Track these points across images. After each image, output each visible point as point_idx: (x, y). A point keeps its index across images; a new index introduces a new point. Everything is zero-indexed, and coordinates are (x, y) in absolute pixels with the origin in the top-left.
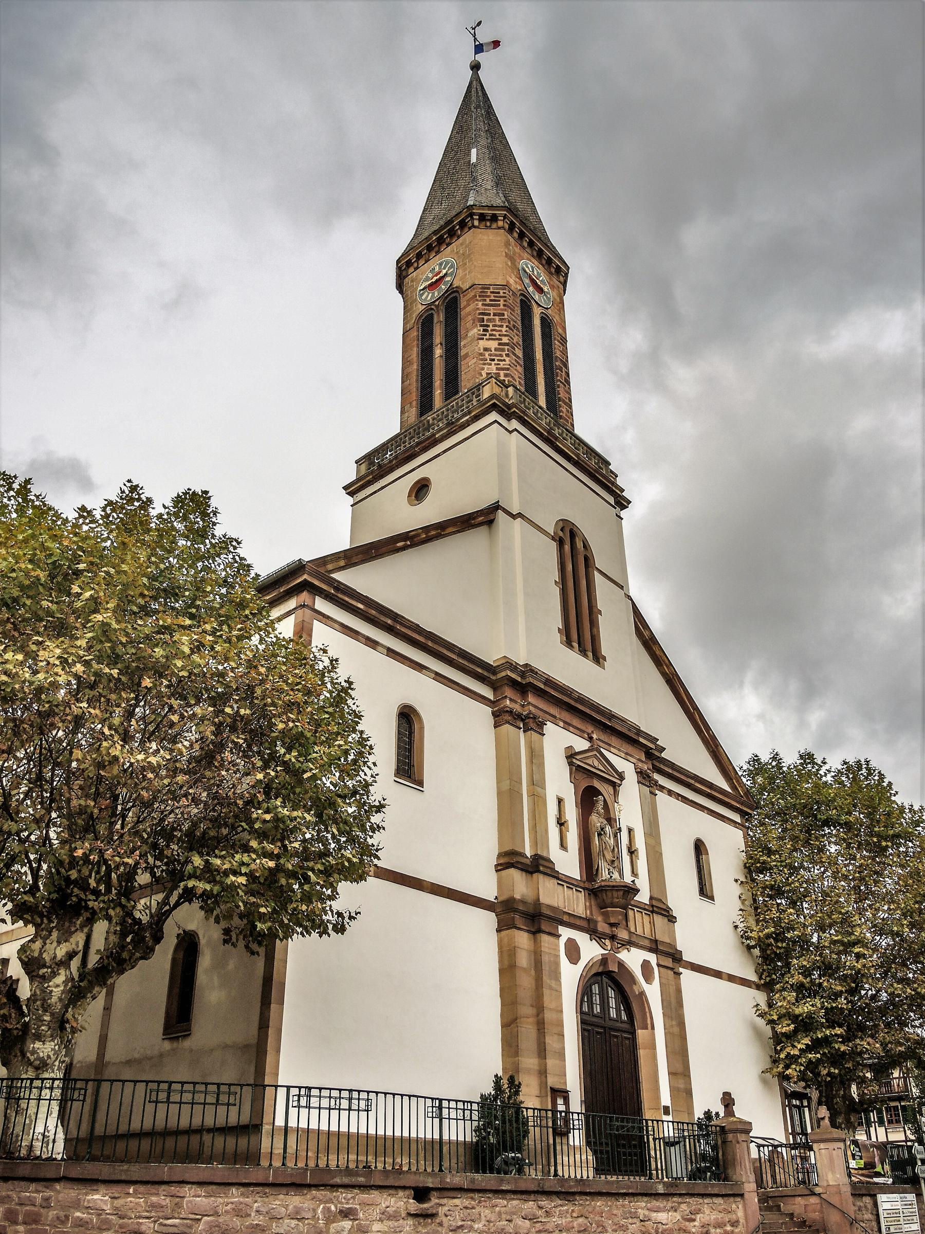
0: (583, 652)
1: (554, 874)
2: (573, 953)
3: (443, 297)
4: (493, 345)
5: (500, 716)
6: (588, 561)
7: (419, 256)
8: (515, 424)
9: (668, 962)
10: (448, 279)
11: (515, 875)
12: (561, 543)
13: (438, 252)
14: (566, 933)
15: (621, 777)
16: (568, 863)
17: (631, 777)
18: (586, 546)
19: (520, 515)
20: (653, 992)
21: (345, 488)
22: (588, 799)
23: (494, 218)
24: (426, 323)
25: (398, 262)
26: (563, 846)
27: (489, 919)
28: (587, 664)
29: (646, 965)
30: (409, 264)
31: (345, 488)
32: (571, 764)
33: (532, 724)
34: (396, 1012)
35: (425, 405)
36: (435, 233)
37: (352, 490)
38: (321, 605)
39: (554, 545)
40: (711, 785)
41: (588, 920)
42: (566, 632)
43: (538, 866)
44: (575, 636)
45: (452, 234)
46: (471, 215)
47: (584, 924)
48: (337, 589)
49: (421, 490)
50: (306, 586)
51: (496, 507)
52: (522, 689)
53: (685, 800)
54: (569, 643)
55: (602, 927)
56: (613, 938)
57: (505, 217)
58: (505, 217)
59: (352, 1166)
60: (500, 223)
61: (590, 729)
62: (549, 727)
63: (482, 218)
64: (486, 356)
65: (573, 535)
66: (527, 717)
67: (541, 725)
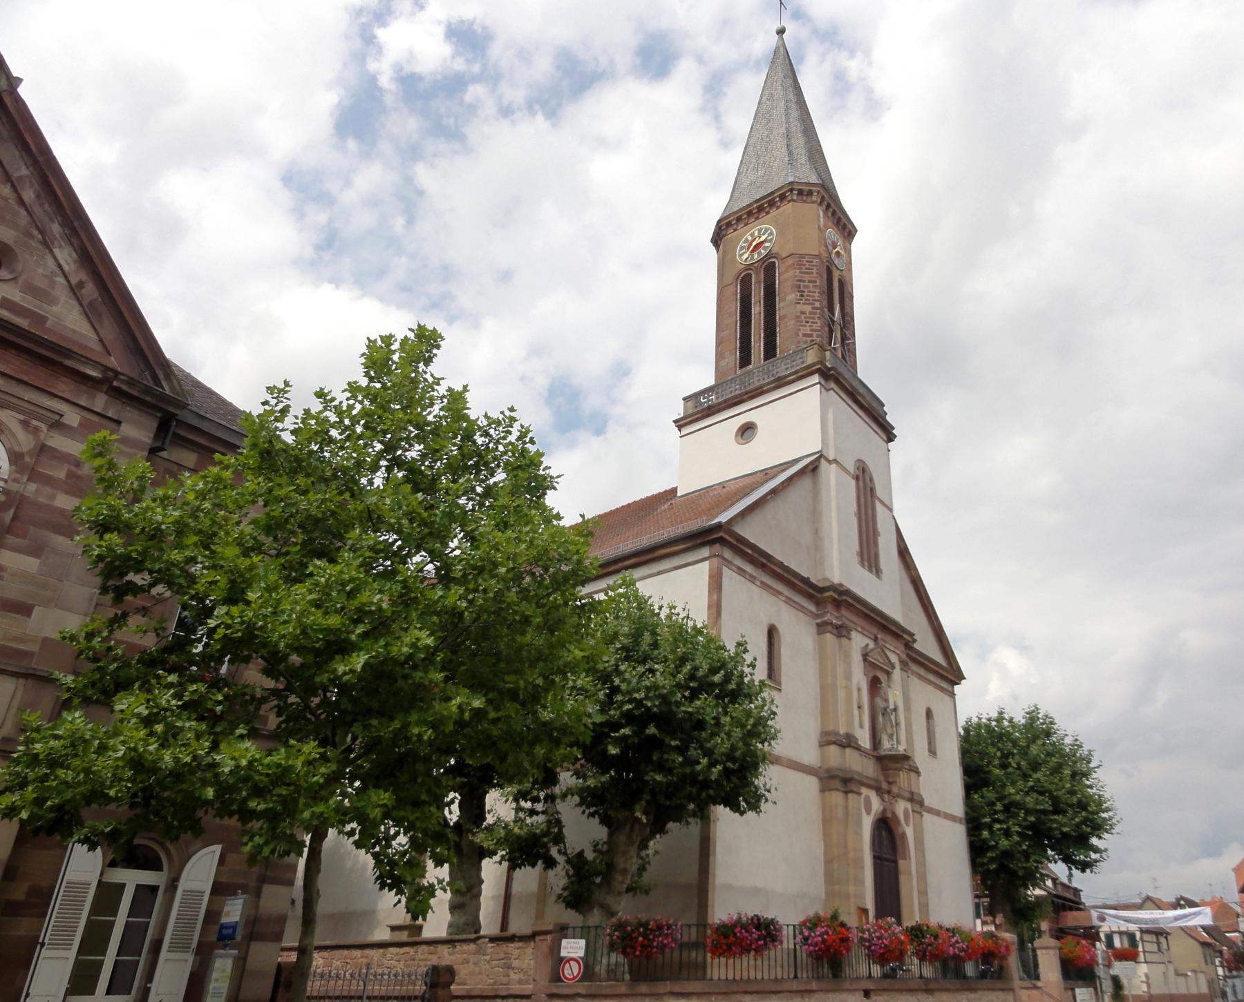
0: (870, 571)
1: (858, 748)
3: (762, 260)
4: (808, 308)
5: (822, 628)
6: (872, 490)
7: (739, 219)
8: (832, 385)
9: (917, 808)
10: (767, 244)
11: (833, 749)
12: (857, 478)
13: (757, 218)
14: (864, 791)
15: (893, 668)
16: (865, 740)
17: (898, 666)
18: (871, 480)
19: (835, 461)
20: (909, 832)
21: (675, 422)
22: (875, 684)
23: (810, 193)
24: (746, 282)
25: (719, 221)
26: (861, 726)
27: (812, 783)
28: (873, 577)
29: (906, 812)
30: (729, 225)
31: (675, 422)
32: (865, 660)
33: (841, 631)
34: (769, 858)
35: (745, 360)
36: (757, 201)
37: (680, 424)
38: (728, 554)
39: (853, 482)
40: (938, 664)
41: (877, 780)
42: (861, 554)
44: (865, 556)
45: (772, 204)
46: (791, 190)
47: (872, 783)
48: (738, 540)
49: (747, 431)
50: (721, 541)
51: (821, 456)
52: (837, 604)
53: (659, 573)
54: (863, 566)
55: (885, 786)
56: (889, 792)
57: (818, 192)
58: (818, 192)
59: (779, 977)
60: (814, 198)
61: (875, 630)
62: (854, 634)
63: (800, 192)
64: (796, 311)
65: (864, 471)
66: (841, 626)
67: (849, 631)
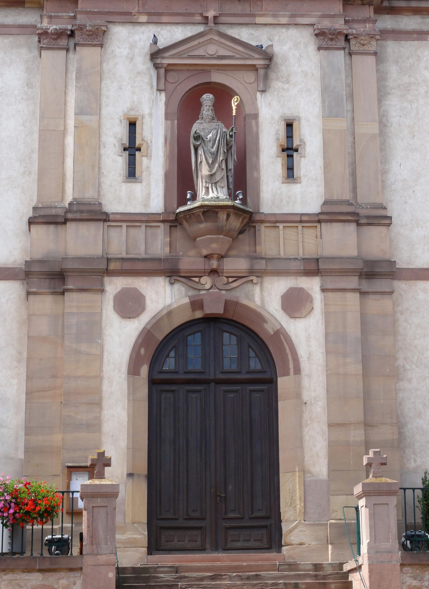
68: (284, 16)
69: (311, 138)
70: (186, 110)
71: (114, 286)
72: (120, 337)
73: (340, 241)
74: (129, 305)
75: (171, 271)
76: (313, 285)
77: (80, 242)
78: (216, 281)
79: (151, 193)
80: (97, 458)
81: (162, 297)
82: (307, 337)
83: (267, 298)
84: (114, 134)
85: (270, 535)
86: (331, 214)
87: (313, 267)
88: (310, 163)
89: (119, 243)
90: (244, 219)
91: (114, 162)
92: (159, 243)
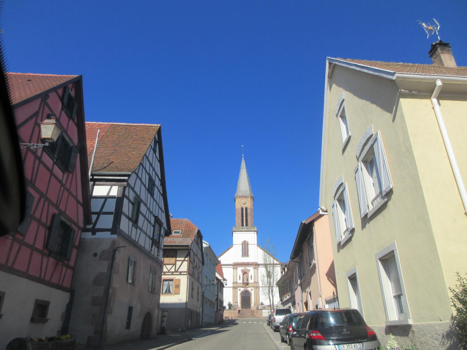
2: (240, 290)
43: (236, 283)
68: (235, 296)
69: (253, 276)
70: (244, 274)
71: (239, 288)
72: (239, 293)
73: (255, 285)
74: (240, 290)
75: (243, 287)
76: (253, 288)
77: (236, 285)
78: (283, 272)
79: (241, 281)
80: (235, 234)
81: (242, 289)
82: (253, 292)
83: (249, 289)
84: (238, 277)
85: (250, 308)
86: (255, 282)
87: (253, 287)
88: (253, 278)
89: (239, 285)
90: (248, 284)
91: (238, 279)
92: (242, 285)
